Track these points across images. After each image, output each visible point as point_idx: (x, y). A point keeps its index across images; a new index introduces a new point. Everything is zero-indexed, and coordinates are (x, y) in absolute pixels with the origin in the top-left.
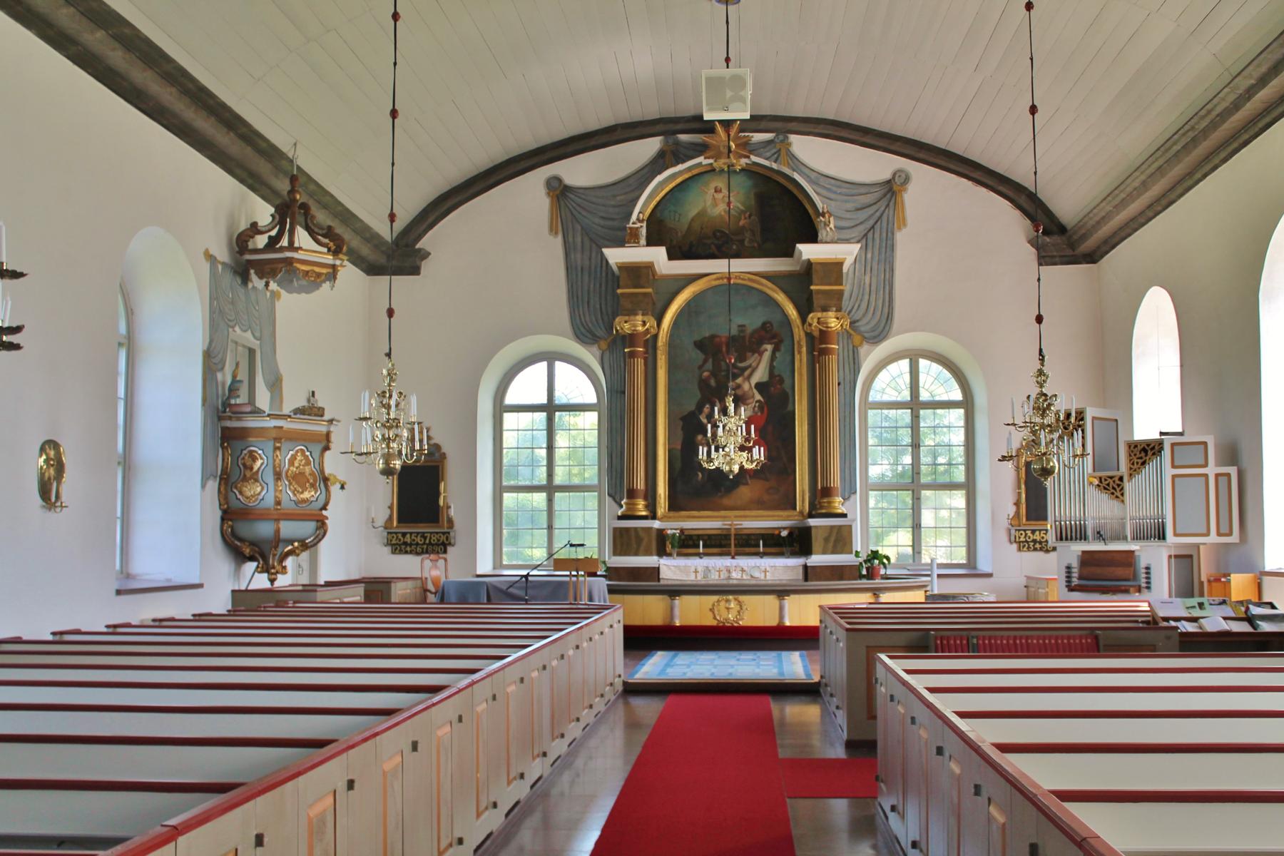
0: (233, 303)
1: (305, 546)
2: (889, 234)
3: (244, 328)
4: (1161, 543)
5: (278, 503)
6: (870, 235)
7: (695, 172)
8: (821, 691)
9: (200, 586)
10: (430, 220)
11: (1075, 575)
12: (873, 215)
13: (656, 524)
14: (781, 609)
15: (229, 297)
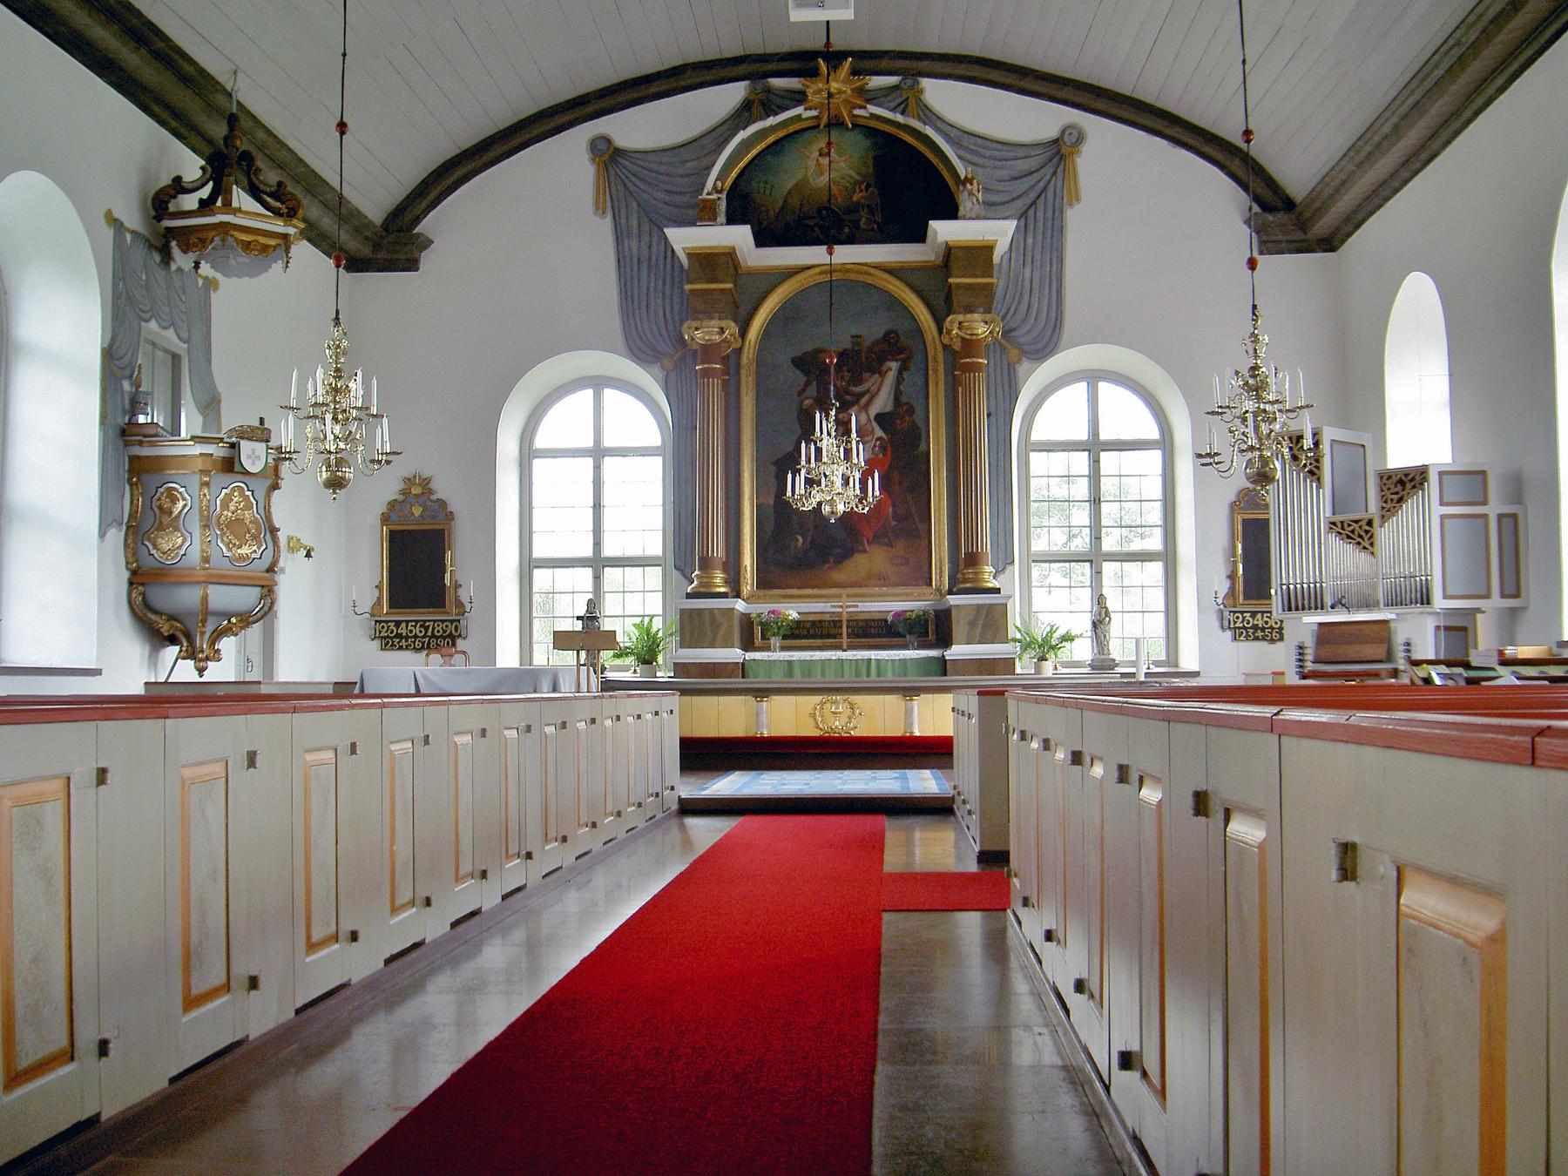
0: (148, 288)
1: (246, 620)
2: (1057, 213)
3: (163, 324)
4: (1426, 609)
5: (206, 560)
6: (1031, 213)
8: (955, 807)
10: (432, 196)
11: (1309, 657)
13: (740, 605)
14: (908, 713)
15: (141, 279)
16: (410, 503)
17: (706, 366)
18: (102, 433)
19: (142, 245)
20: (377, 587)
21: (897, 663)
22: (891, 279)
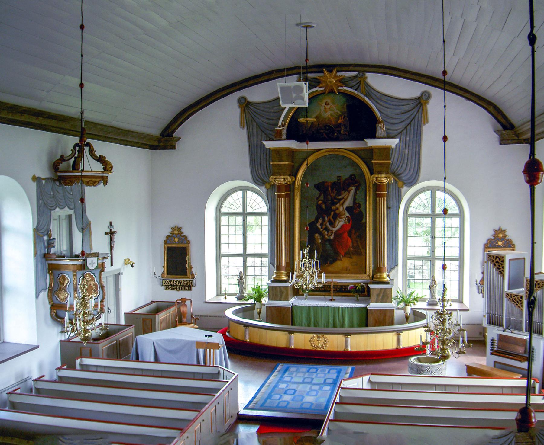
2: (419, 127)
6: (409, 127)
7: (315, 94)
9: (38, 347)
12: (410, 116)
14: (346, 342)
16: (174, 237)
17: (279, 193)
18: (35, 260)
19: (50, 182)
20: (163, 267)
21: (349, 308)
22: (353, 154)
